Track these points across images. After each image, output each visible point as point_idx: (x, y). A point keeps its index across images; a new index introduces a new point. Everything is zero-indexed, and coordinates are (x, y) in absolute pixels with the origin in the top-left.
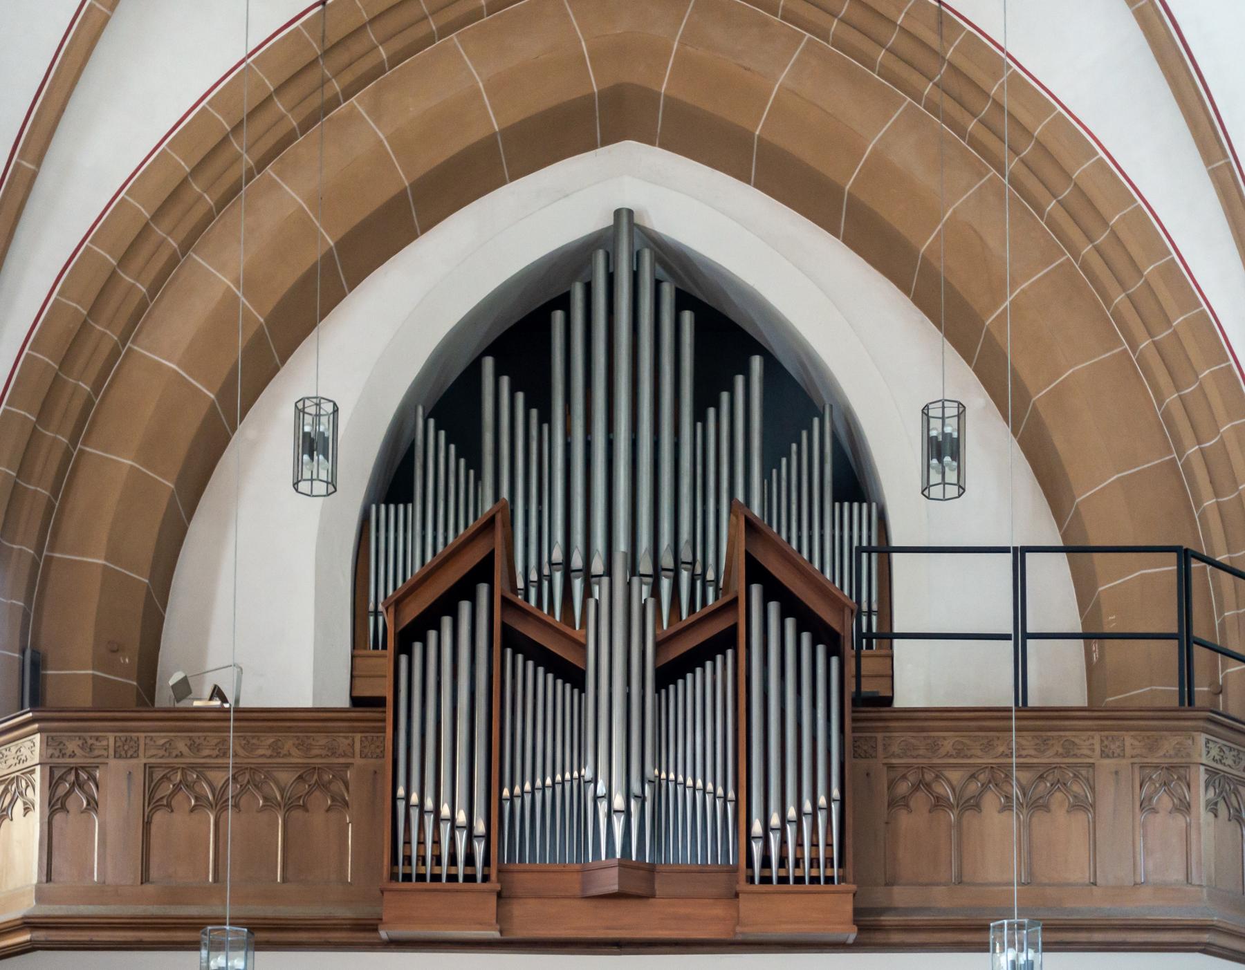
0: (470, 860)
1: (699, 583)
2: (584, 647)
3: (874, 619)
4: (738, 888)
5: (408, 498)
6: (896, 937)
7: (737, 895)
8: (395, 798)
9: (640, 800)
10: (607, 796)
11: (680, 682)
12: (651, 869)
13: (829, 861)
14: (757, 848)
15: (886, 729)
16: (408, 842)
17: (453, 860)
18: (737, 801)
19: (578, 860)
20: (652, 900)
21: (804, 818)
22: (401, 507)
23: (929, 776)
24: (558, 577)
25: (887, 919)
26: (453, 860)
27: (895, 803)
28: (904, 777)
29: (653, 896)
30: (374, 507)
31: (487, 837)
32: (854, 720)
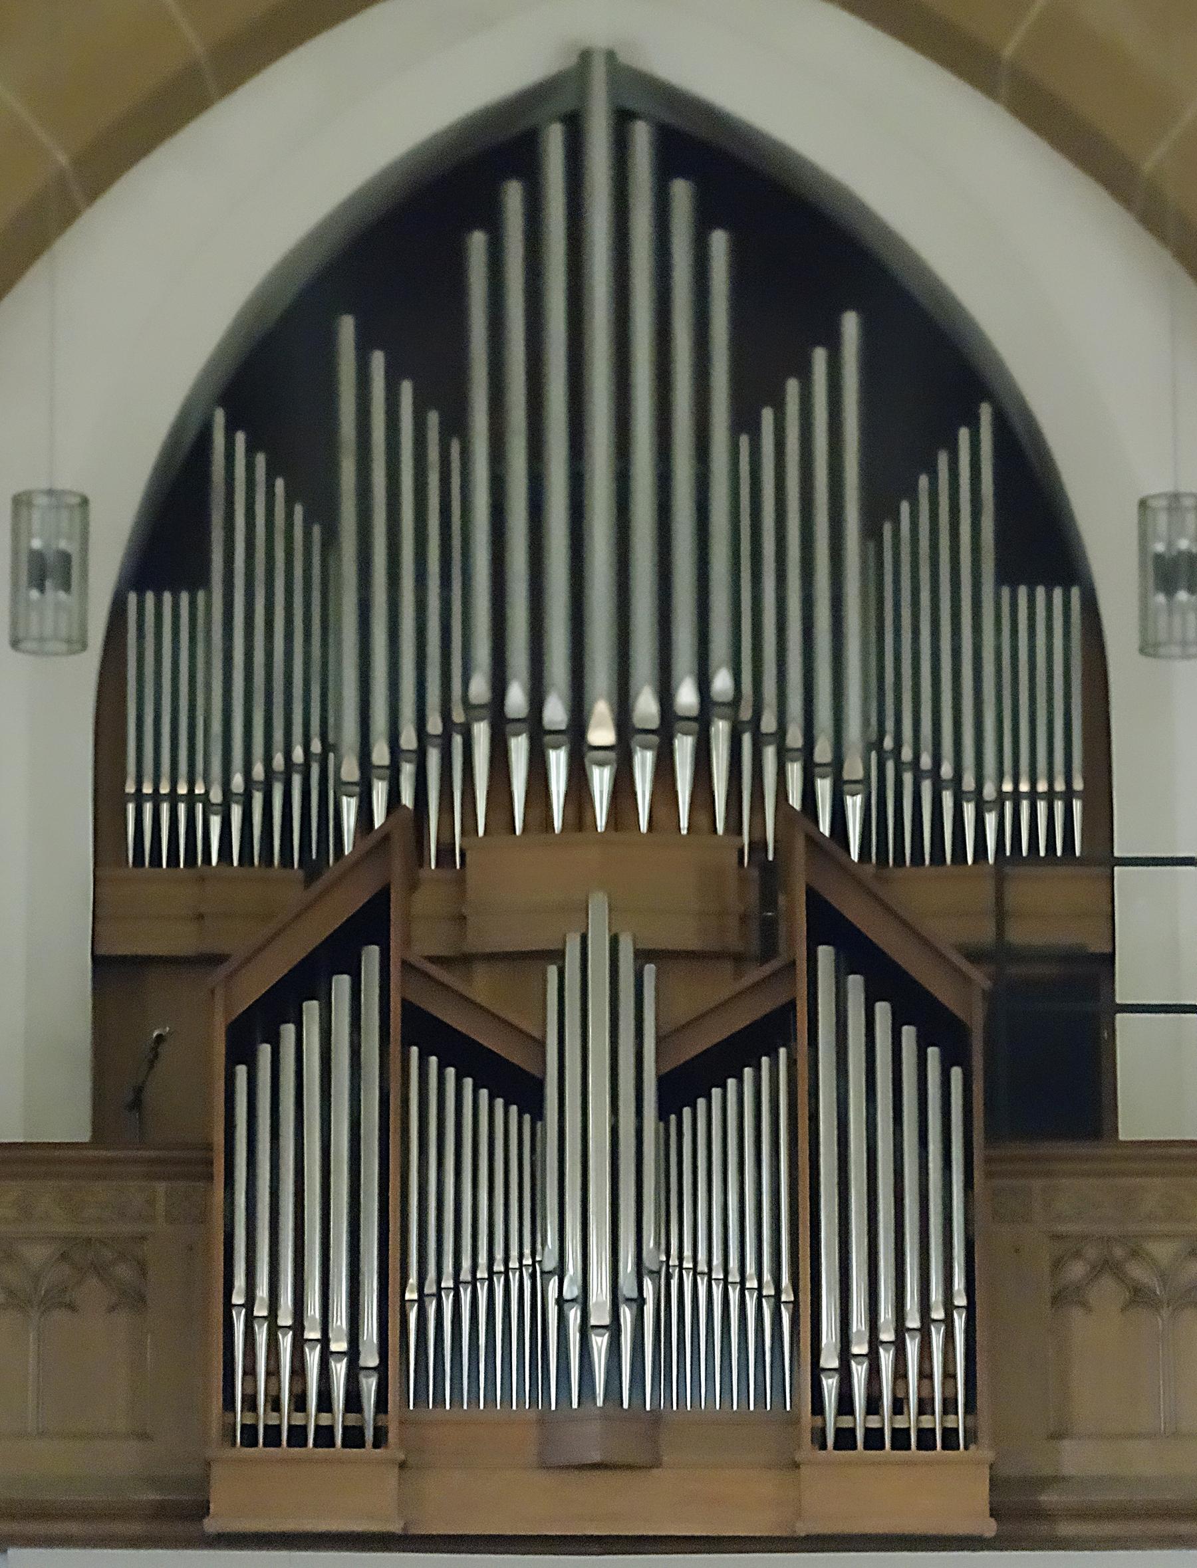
0: (353, 1401)
1: (747, 739)
2: (542, 1044)
3: (1077, 806)
4: (798, 1457)
5: (197, 579)
6: (1066, 1529)
7: (797, 1466)
8: (228, 1306)
9: (634, 1306)
10: (580, 1300)
11: (701, 1103)
12: (656, 1418)
13: (949, 1406)
14: (830, 1384)
15: (1049, 1174)
16: (250, 1371)
17: (325, 1403)
18: (796, 1303)
19: (533, 1401)
20: (655, 1472)
21: (907, 1335)
22: (184, 597)
23: (1119, 1252)
24: (481, 732)
25: (1048, 1498)
26: (325, 1403)
27: (1062, 1298)
28: (1078, 1255)
29: (656, 1464)
30: (132, 598)
31: (382, 1370)
32: (988, 1160)
